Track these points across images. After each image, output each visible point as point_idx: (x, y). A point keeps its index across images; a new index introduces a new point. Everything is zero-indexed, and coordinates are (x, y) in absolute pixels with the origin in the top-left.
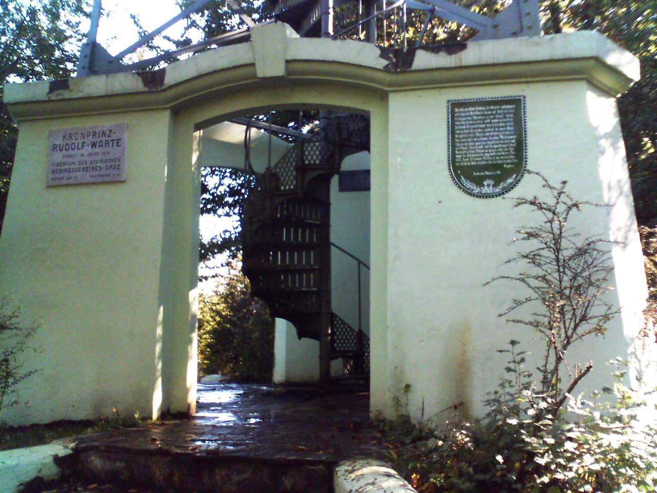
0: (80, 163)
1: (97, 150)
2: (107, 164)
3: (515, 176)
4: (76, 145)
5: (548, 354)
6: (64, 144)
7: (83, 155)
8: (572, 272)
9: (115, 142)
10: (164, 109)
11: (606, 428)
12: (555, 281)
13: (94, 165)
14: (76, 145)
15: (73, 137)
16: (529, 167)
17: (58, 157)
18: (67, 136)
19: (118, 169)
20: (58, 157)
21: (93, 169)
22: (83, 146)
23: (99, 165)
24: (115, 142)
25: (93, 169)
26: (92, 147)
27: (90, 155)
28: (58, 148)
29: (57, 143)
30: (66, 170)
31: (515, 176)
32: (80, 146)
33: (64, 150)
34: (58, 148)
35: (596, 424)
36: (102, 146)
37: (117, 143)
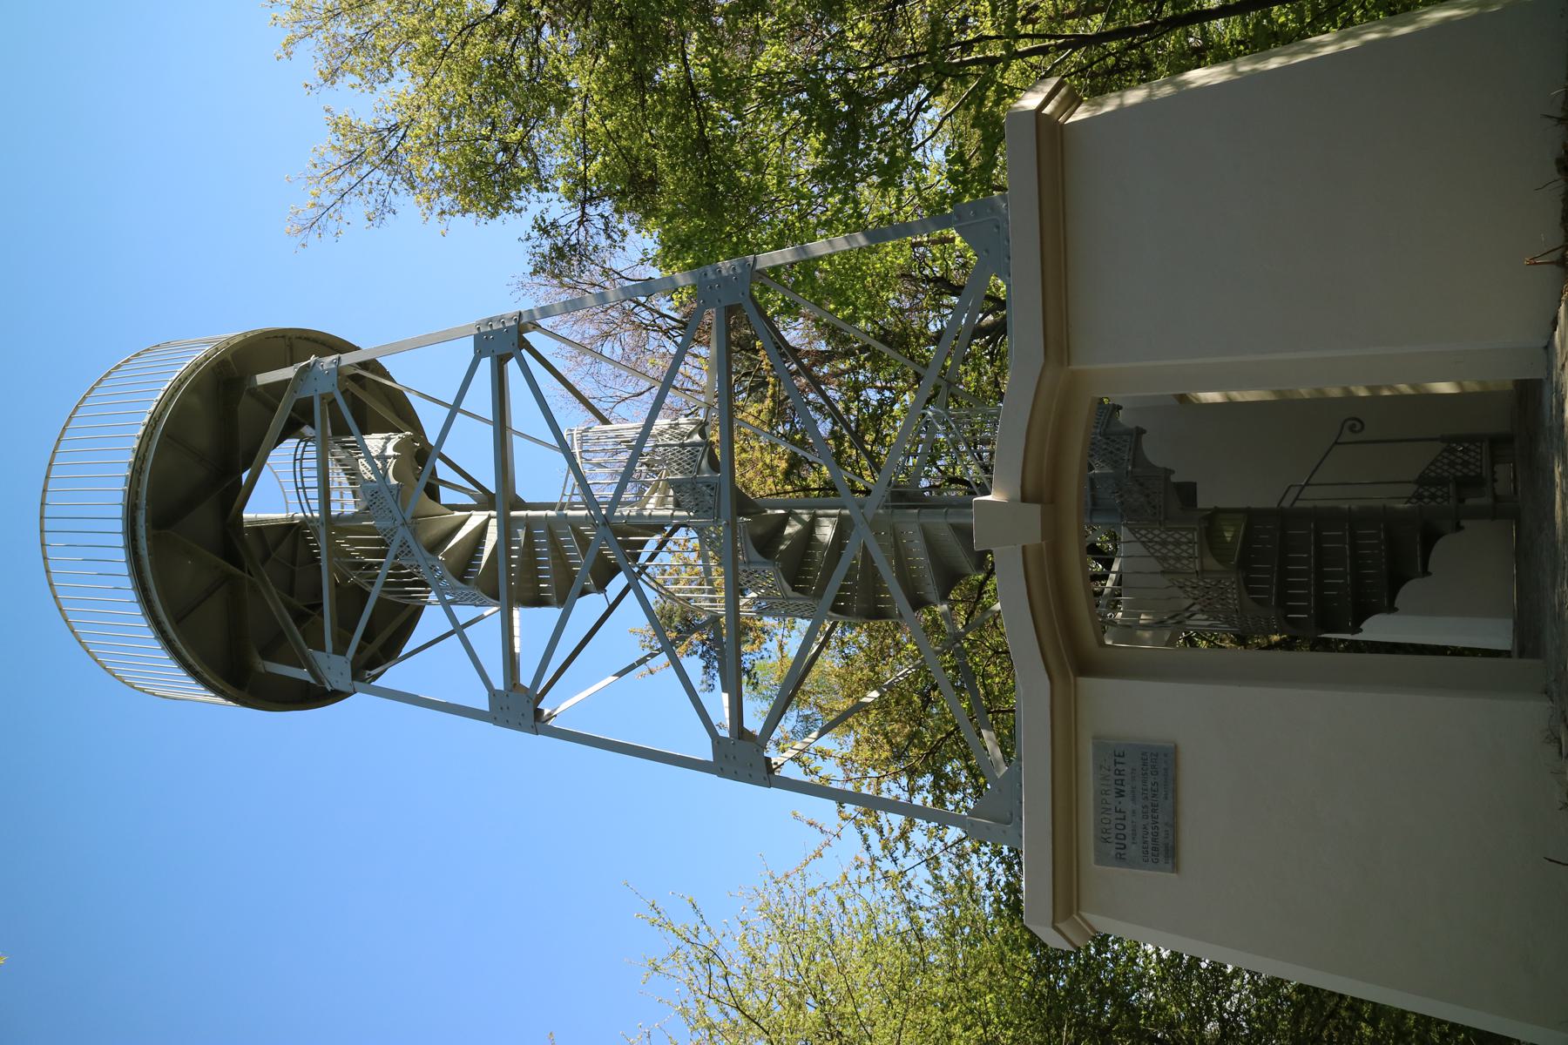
0: (1145, 816)
1: (1127, 788)
2: (1149, 772)
3: (1084, 49)
4: (1119, 822)
5: (782, 652)
6: (1116, 841)
7: (1134, 812)
8: (586, 168)
9: (1118, 759)
10: (1075, 682)
11: (1345, 40)
12: (920, 136)
13: (1150, 794)
14: (1119, 822)
15: (1107, 826)
16: (121, 521)
17: (1134, 850)
18: (1105, 836)
19: (1157, 755)
20: (1134, 850)
21: (1154, 796)
22: (1120, 811)
23: (1150, 786)
24: (1118, 759)
25: (1154, 796)
26: (1123, 796)
27: (1134, 799)
28: (1122, 852)
29: (1113, 853)
30: (1154, 840)
31: (1084, 49)
32: (1121, 816)
33: (1125, 842)
34: (1122, 852)
35: (899, 992)
36: (1122, 780)
37: (1119, 756)
